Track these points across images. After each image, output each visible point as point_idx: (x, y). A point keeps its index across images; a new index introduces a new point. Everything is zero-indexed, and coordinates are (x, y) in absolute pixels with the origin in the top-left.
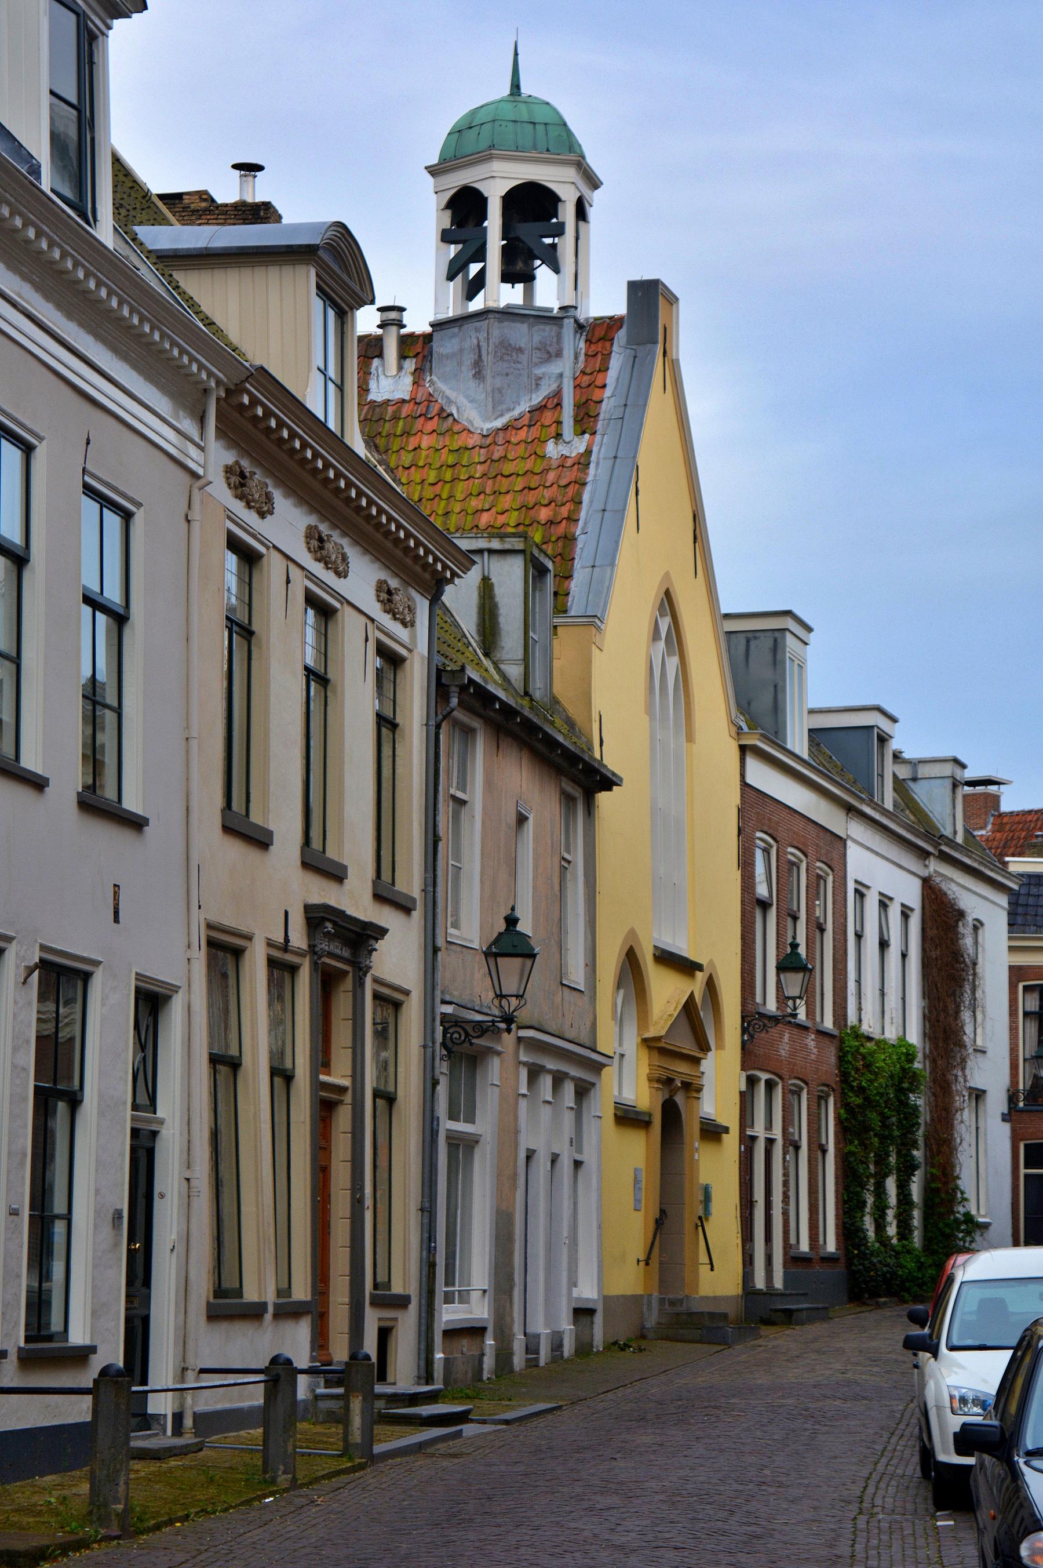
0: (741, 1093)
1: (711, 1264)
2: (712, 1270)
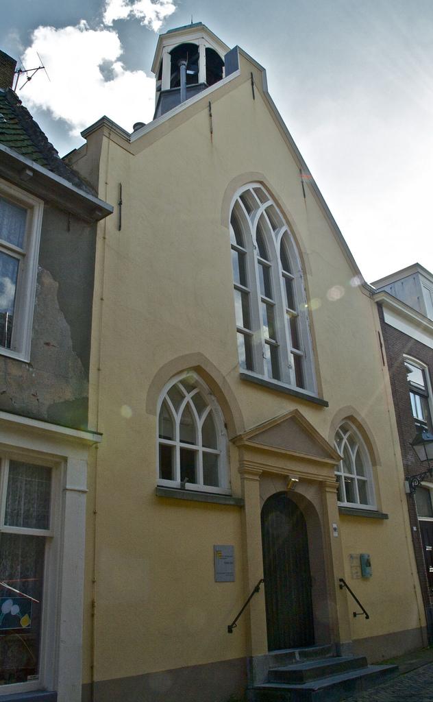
0: (407, 494)
1: (365, 612)
2: (367, 617)
